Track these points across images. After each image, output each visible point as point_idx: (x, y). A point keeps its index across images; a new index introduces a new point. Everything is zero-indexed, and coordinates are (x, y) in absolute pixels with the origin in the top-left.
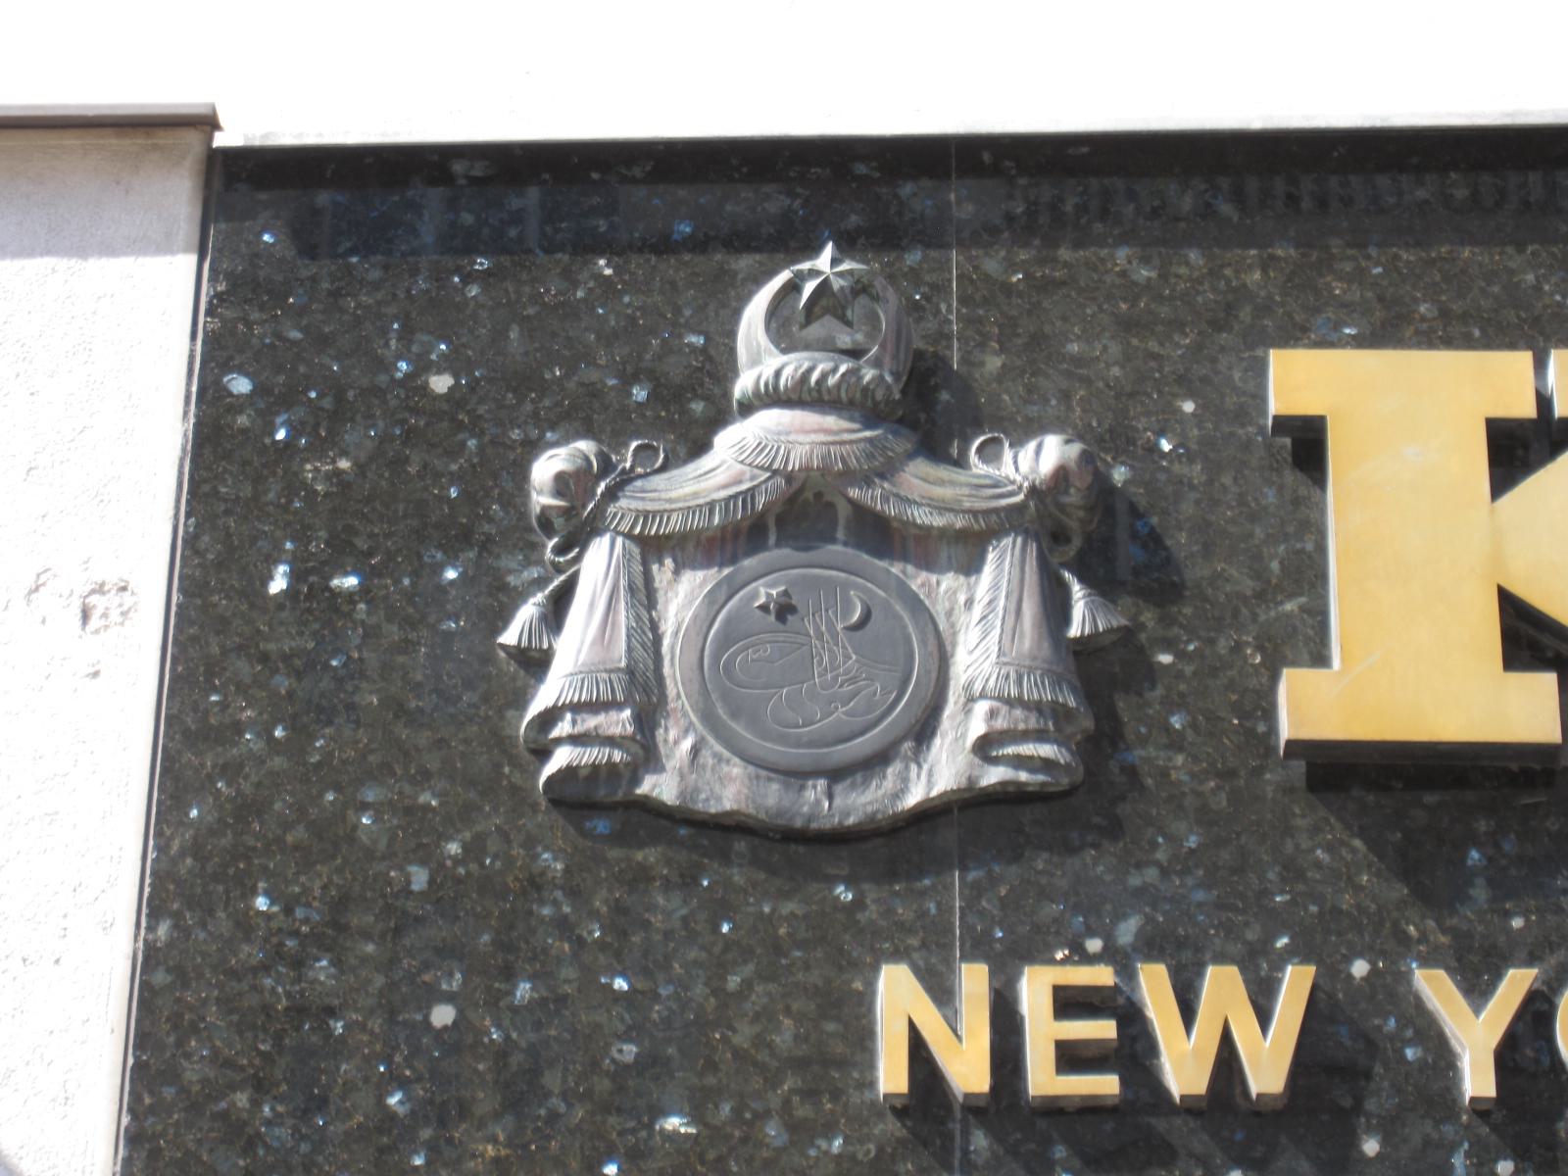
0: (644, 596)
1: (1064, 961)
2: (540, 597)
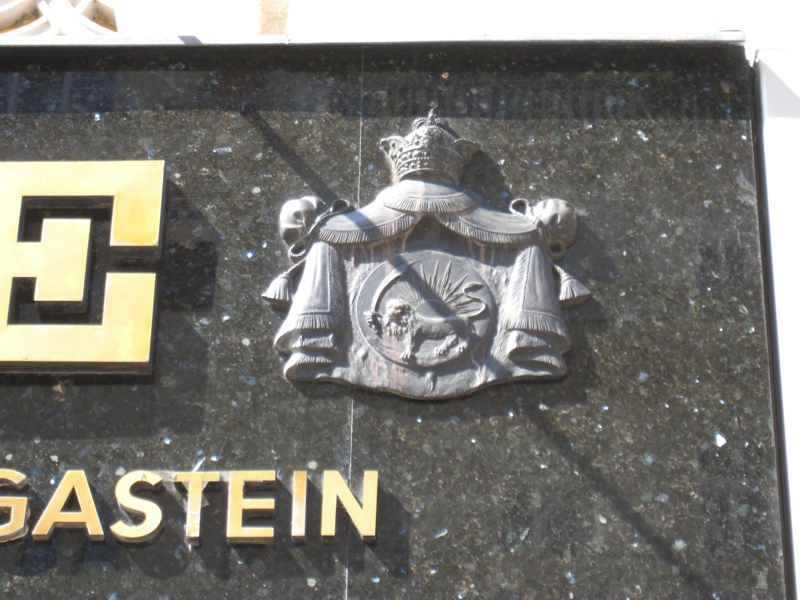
0: (341, 277)
1: (58, 481)
2: (285, 274)
